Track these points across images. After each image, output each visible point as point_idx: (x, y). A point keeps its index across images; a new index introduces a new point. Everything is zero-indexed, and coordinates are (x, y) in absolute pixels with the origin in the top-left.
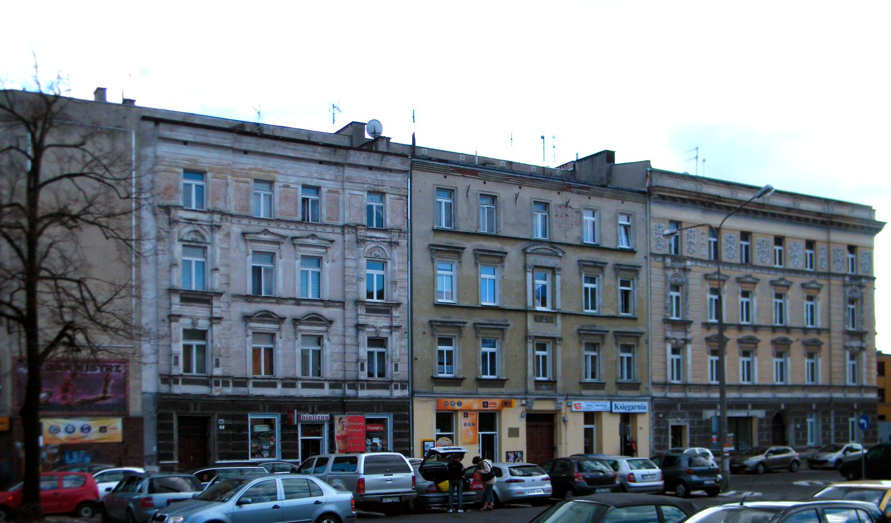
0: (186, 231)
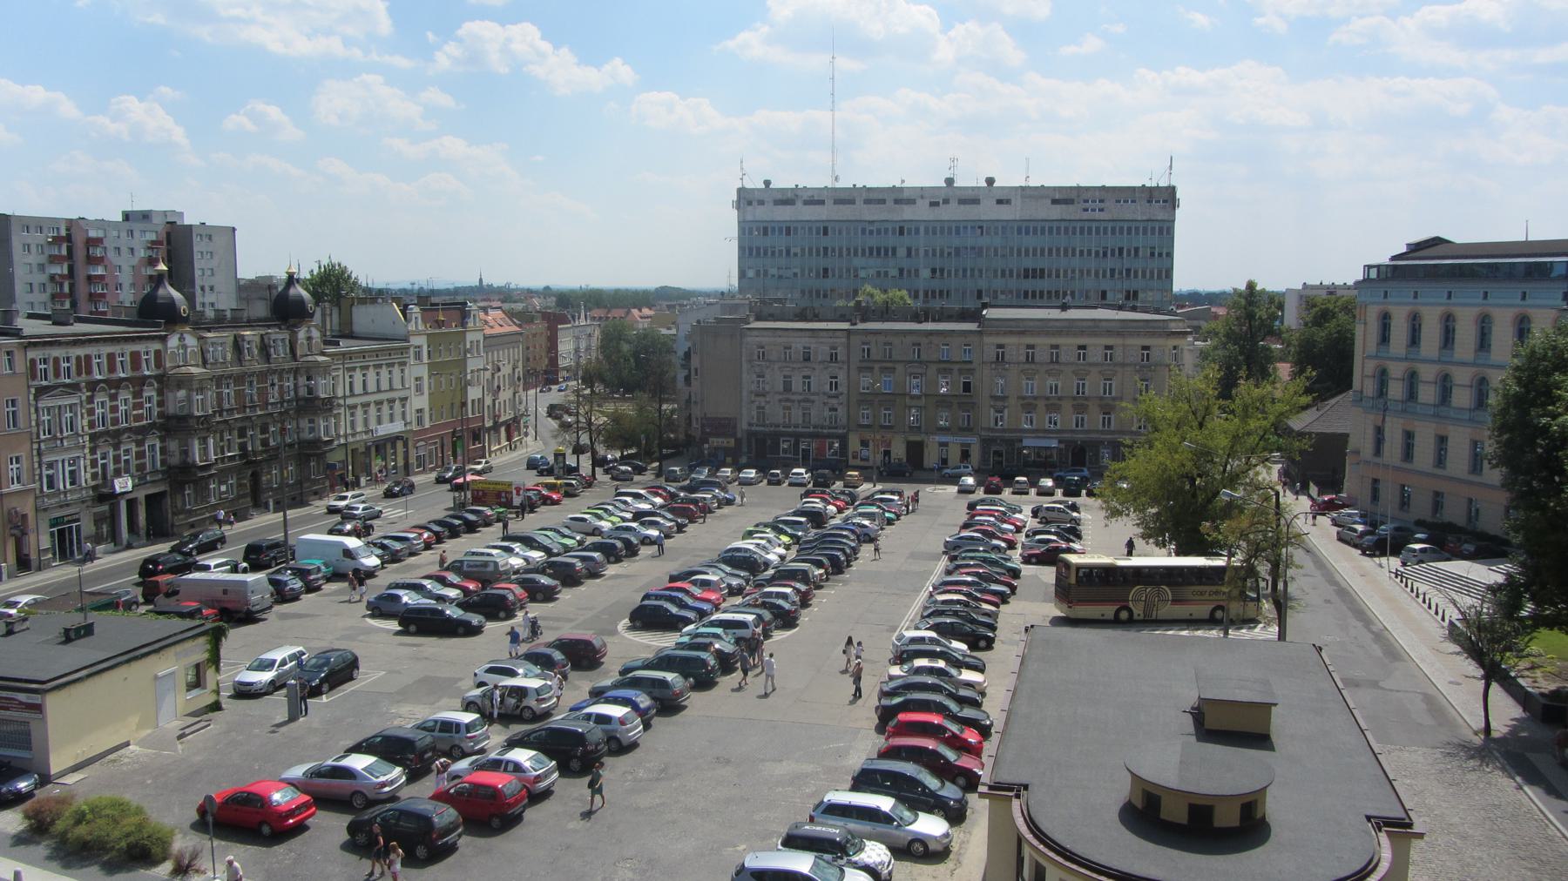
0: (757, 370)
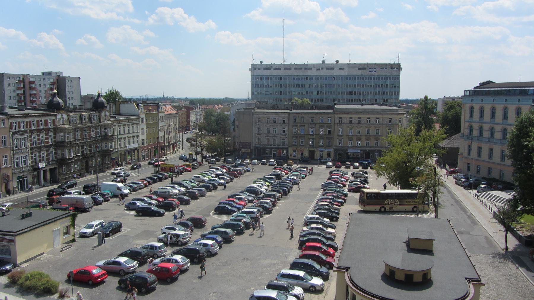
0: (258, 126)
